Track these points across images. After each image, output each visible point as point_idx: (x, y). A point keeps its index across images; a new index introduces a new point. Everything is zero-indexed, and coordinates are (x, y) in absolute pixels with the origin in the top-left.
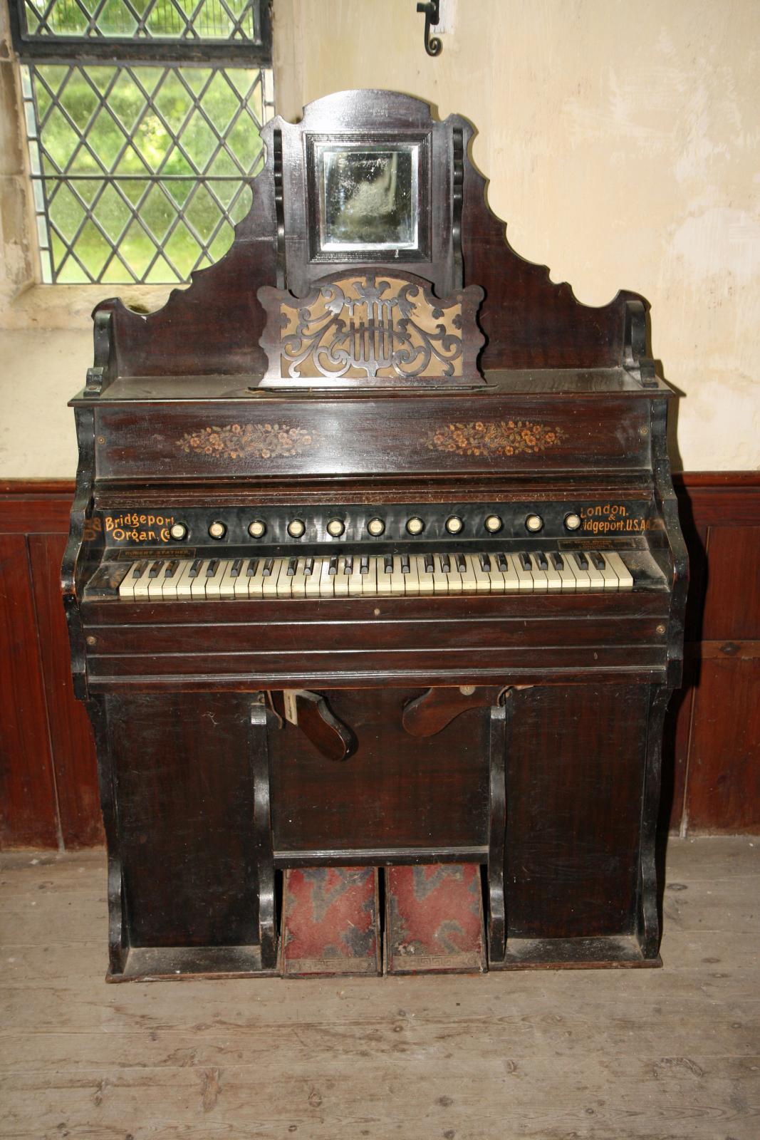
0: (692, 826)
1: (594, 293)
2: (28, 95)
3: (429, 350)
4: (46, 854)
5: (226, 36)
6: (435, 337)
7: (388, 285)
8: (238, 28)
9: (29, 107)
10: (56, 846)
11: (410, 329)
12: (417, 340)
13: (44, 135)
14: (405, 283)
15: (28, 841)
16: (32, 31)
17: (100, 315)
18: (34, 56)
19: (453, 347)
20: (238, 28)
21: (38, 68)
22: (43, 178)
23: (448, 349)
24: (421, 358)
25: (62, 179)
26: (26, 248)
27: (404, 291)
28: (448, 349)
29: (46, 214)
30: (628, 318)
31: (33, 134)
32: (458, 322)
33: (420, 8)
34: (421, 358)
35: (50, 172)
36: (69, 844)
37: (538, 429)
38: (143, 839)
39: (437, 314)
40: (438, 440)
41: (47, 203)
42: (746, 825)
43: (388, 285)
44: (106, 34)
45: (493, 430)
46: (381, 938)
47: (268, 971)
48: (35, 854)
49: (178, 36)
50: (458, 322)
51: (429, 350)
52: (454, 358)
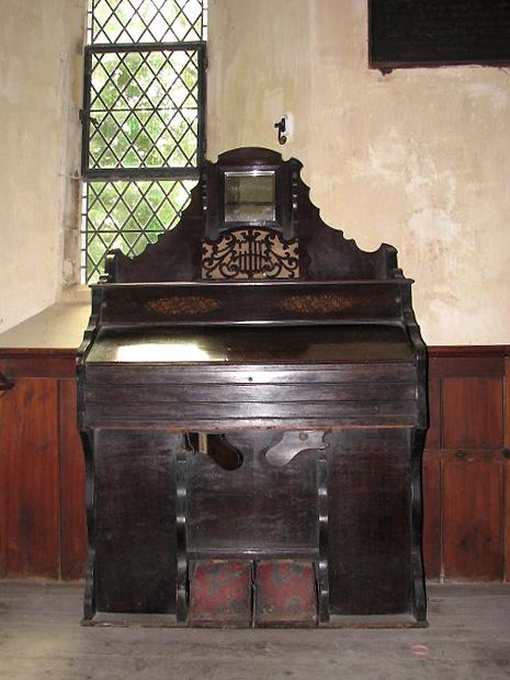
0: (448, 576)
1: (368, 245)
2: (85, 194)
3: (281, 265)
4: (53, 581)
5: (183, 165)
6: (284, 259)
7: (259, 234)
8: (189, 162)
9: (84, 200)
10: (56, 578)
11: (271, 255)
12: (275, 260)
13: (96, 10)
14: (267, 233)
15: (41, 574)
16: (91, 167)
17: (109, 256)
18: (90, 178)
19: (294, 264)
20: (189, 162)
21: (92, 184)
22: (87, 232)
23: (291, 264)
24: (277, 269)
25: (97, 232)
26: (74, 265)
27: (268, 236)
28: (291, 264)
29: (86, 250)
30: (388, 254)
31: (84, 211)
32: (296, 251)
33: (276, 125)
34: (277, 269)
35: (91, 229)
36: (64, 579)
37: (340, 299)
38: (109, 537)
39: (284, 249)
40: (286, 304)
41: (87, 245)
42: (480, 575)
43: (259, 234)
44: (125, 167)
45: (316, 300)
46: (253, 608)
47: (182, 624)
48: (43, 581)
49: (160, 166)
50: (296, 251)
51: (281, 265)
52: (295, 268)
